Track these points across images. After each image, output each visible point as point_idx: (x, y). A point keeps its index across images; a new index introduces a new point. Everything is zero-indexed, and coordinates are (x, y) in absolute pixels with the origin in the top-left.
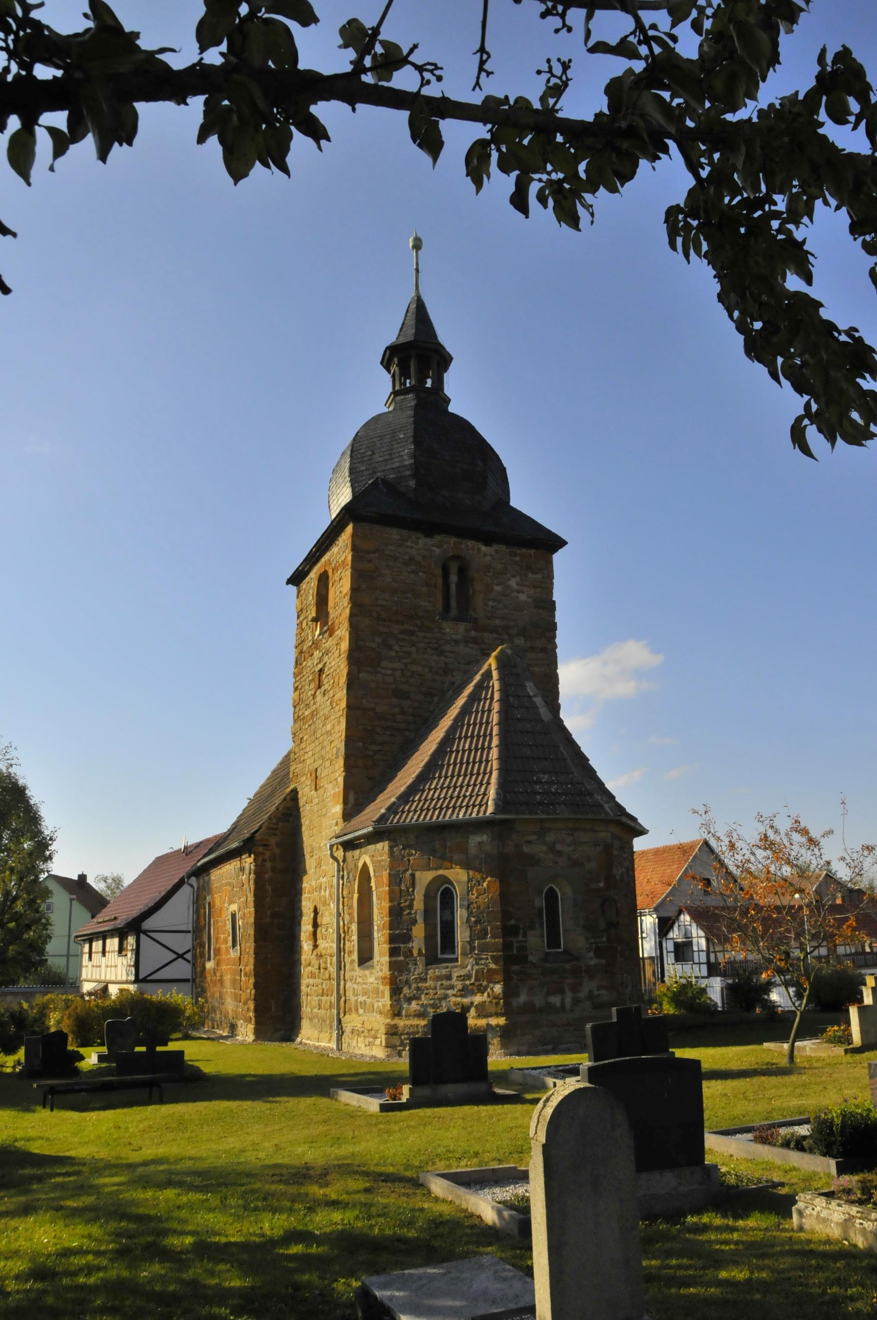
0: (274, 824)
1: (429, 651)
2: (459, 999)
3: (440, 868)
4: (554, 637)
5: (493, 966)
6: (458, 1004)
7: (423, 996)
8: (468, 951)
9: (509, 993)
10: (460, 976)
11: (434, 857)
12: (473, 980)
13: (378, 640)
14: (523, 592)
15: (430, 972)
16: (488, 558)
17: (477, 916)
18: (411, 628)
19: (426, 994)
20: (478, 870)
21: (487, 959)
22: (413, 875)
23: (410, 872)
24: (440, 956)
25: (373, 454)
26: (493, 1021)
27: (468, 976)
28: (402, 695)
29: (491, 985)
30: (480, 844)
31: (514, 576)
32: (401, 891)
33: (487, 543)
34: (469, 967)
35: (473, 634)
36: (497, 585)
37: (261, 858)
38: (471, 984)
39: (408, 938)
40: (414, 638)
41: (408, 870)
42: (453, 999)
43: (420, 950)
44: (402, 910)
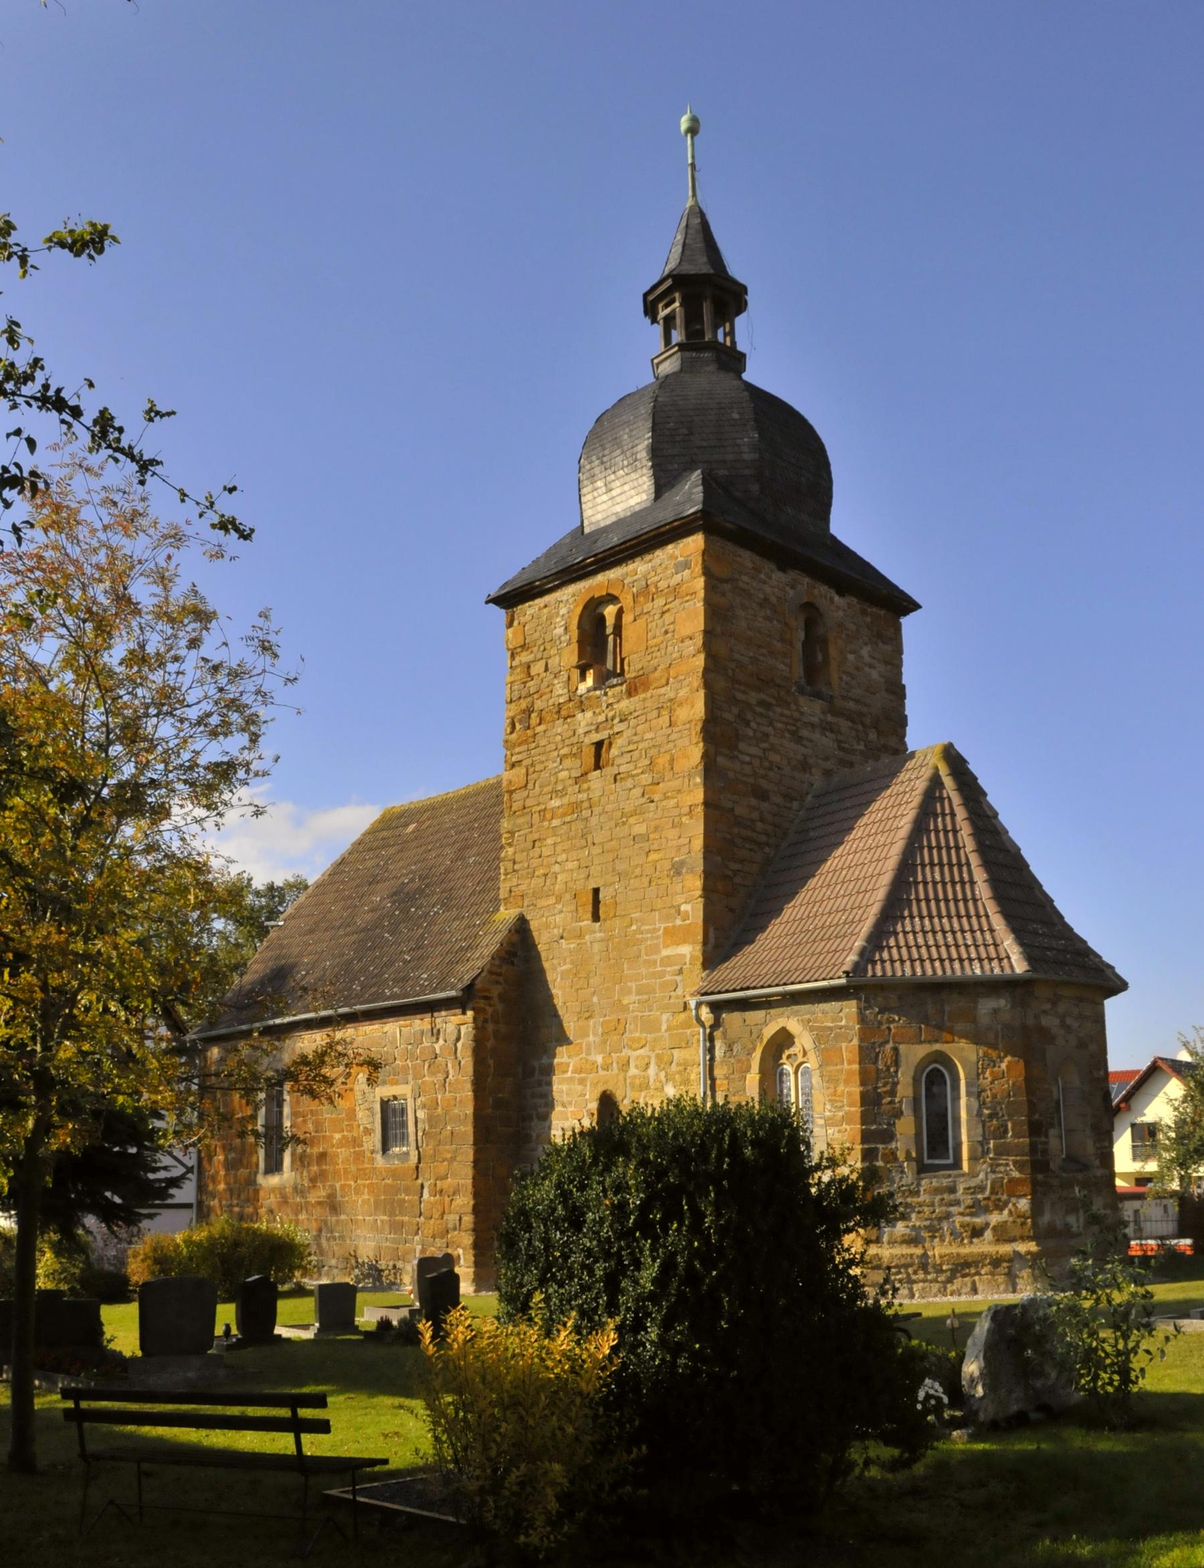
1: (787, 735)
2: (968, 1219)
3: (937, 1041)
4: (904, 735)
5: (1016, 1174)
6: (968, 1225)
7: (913, 1216)
9: (1036, 1209)
10: (969, 1188)
11: (927, 1025)
12: (987, 1193)
13: (735, 710)
15: (923, 1182)
16: (841, 613)
17: (993, 1108)
19: (919, 1212)
20: (994, 1046)
21: (1007, 1165)
22: (896, 1050)
23: (891, 1045)
24: (927, 1161)
25: (691, 433)
26: (1023, 1247)
27: (981, 1189)
28: (763, 796)
29: (1013, 1200)
30: (996, 1011)
31: (866, 644)
32: (878, 1069)
33: (841, 593)
34: (982, 1176)
35: (829, 718)
36: (851, 653)
37: (481, 1018)
38: (985, 1199)
40: (771, 714)
41: (887, 1042)
42: (958, 1219)
43: (908, 1153)
44: (880, 1097)
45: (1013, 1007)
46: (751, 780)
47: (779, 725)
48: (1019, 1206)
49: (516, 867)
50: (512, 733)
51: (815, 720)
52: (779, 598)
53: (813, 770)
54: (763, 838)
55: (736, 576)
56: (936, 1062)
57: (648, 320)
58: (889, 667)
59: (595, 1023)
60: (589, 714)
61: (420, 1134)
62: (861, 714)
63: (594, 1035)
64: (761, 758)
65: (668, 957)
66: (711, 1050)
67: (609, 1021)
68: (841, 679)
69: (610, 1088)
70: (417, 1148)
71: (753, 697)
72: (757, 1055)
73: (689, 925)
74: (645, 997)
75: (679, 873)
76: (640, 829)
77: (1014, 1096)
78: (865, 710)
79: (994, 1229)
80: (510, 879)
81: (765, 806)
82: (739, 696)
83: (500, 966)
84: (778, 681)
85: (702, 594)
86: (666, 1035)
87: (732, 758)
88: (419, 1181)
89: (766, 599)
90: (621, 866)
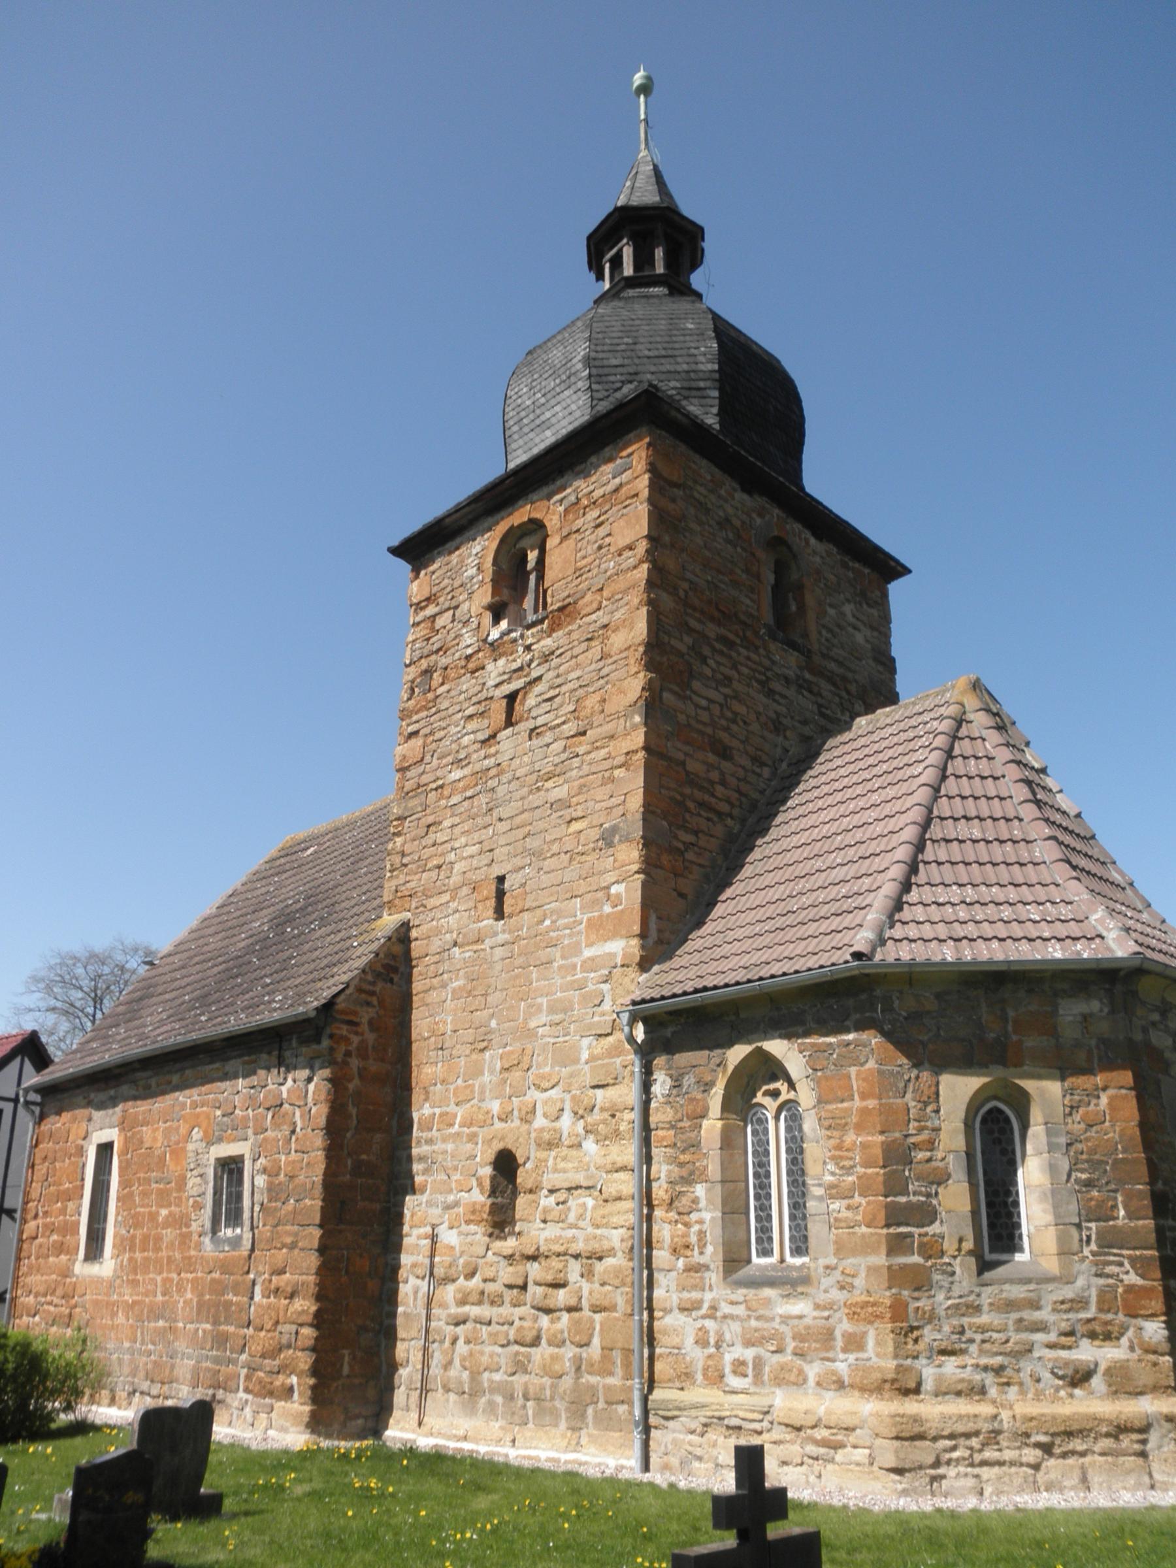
0: (370, 983)
5: (1132, 1278)
7: (973, 1348)
8: (1075, 1246)
13: (689, 640)
14: (859, 630)
18: (731, 636)
24: (989, 1257)
27: (1079, 1303)
28: (724, 753)
31: (848, 601)
34: (1080, 1282)
35: (807, 676)
36: (831, 606)
39: (927, 1214)
45: (1113, 1011)
46: (709, 730)
47: (745, 670)
48: (1146, 1335)
49: (405, 861)
50: (409, 699)
51: (791, 674)
52: (743, 523)
53: (788, 733)
54: (724, 807)
55: (690, 483)
56: (995, 1098)
57: (593, 276)
58: (876, 634)
59: (492, 1057)
60: (502, 662)
61: (257, 1208)
62: (844, 679)
63: (492, 1072)
64: (721, 705)
65: (592, 959)
66: (646, 1086)
67: (512, 1052)
68: (820, 633)
69: (510, 1147)
70: (252, 1228)
71: (712, 630)
72: (718, 1090)
73: (622, 911)
74: (826, 1314)
75: (610, 845)
76: (560, 792)
77: (1124, 1151)
78: (850, 675)
79: (1108, 1372)
80: (397, 877)
81: (726, 765)
82: (693, 623)
83: (374, 983)
84: (743, 618)
85: (646, 493)
86: (587, 1067)
87: (684, 698)
88: (252, 1276)
89: (727, 520)
90: (533, 843)
